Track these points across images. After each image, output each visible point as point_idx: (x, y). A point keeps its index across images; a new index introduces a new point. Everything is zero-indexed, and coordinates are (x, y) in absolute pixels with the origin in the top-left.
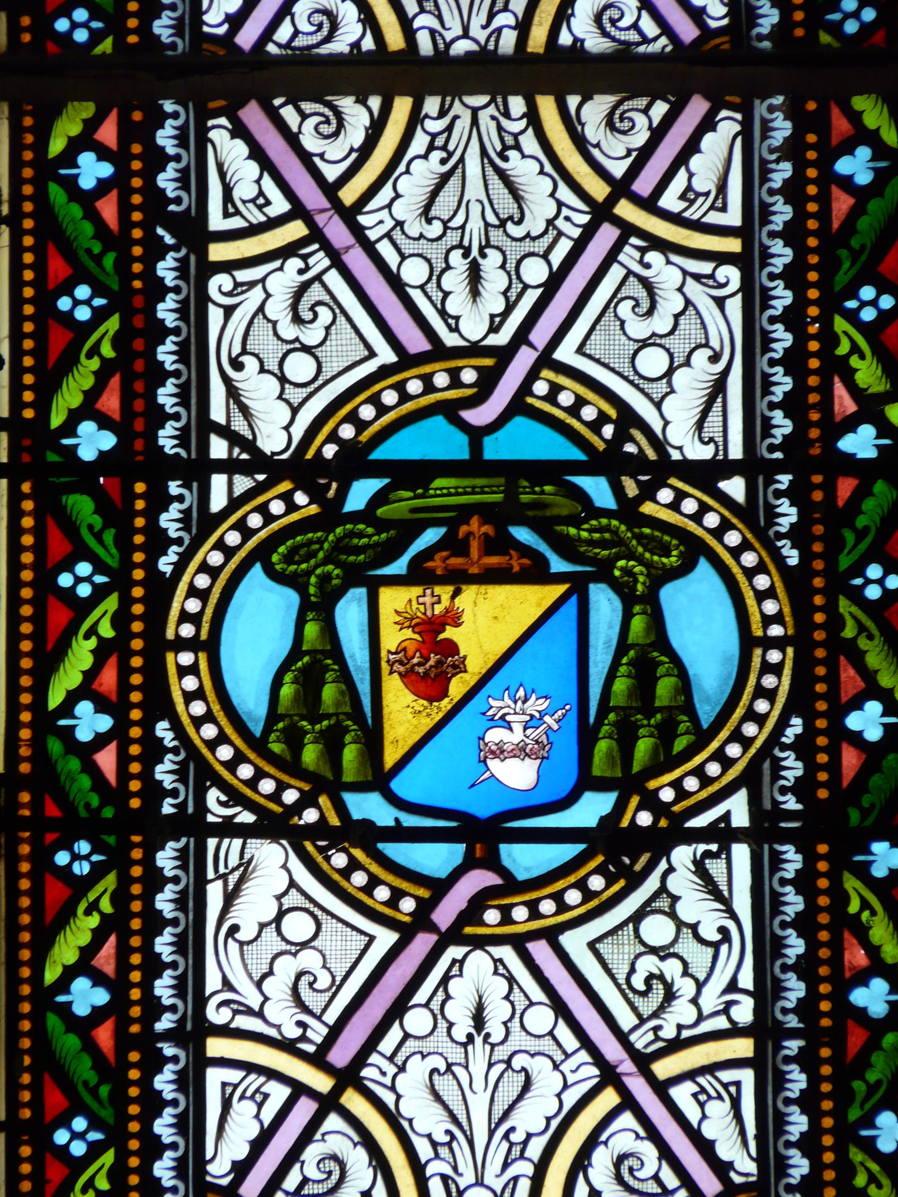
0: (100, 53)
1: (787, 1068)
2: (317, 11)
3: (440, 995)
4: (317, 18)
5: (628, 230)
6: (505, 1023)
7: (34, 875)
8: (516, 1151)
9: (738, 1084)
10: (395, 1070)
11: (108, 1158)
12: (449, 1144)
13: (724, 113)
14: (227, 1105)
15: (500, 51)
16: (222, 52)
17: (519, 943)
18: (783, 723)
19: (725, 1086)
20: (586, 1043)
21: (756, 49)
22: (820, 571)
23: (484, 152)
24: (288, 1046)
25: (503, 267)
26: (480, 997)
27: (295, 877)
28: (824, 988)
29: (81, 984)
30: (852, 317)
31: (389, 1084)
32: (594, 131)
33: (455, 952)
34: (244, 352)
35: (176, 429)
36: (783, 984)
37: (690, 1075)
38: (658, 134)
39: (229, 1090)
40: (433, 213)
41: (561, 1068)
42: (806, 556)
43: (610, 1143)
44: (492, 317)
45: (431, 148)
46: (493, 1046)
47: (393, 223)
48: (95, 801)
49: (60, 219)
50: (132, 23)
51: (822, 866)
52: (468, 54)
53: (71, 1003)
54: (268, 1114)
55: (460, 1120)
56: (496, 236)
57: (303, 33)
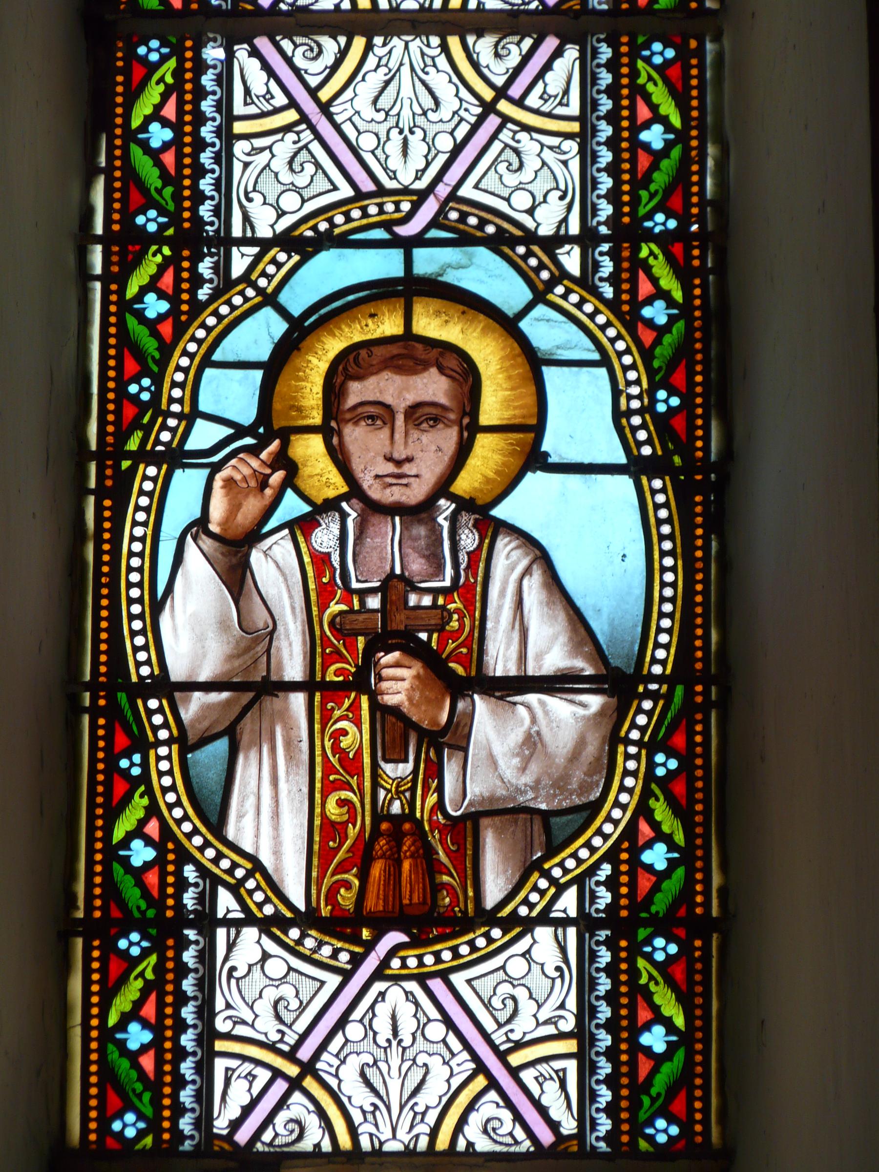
1: (598, 70)
3: (430, 158)
4: (291, 1126)
5: (506, 119)
7: (117, 402)
8: (419, 1117)
9: (564, 1070)
10: (339, 1062)
11: (153, 959)
12: (373, 1113)
13: (225, 1132)
14: (227, 1082)
17: (422, 979)
18: (596, 867)
19: (556, 1072)
20: (337, 127)
23: (388, 1108)
24: (271, 1047)
25: (424, 140)
26: (405, 162)
27: (288, 215)
28: (624, 1012)
30: (649, 957)
31: (463, 102)
32: (312, 1122)
33: (379, 986)
36: (596, 1037)
37: (277, 111)
38: (526, 59)
40: (422, 1071)
42: (617, 292)
43: (480, 1110)
44: (417, 171)
45: (424, 1114)
46: (404, 1049)
47: (354, 112)
48: (143, 906)
51: (626, 188)
56: (420, 121)
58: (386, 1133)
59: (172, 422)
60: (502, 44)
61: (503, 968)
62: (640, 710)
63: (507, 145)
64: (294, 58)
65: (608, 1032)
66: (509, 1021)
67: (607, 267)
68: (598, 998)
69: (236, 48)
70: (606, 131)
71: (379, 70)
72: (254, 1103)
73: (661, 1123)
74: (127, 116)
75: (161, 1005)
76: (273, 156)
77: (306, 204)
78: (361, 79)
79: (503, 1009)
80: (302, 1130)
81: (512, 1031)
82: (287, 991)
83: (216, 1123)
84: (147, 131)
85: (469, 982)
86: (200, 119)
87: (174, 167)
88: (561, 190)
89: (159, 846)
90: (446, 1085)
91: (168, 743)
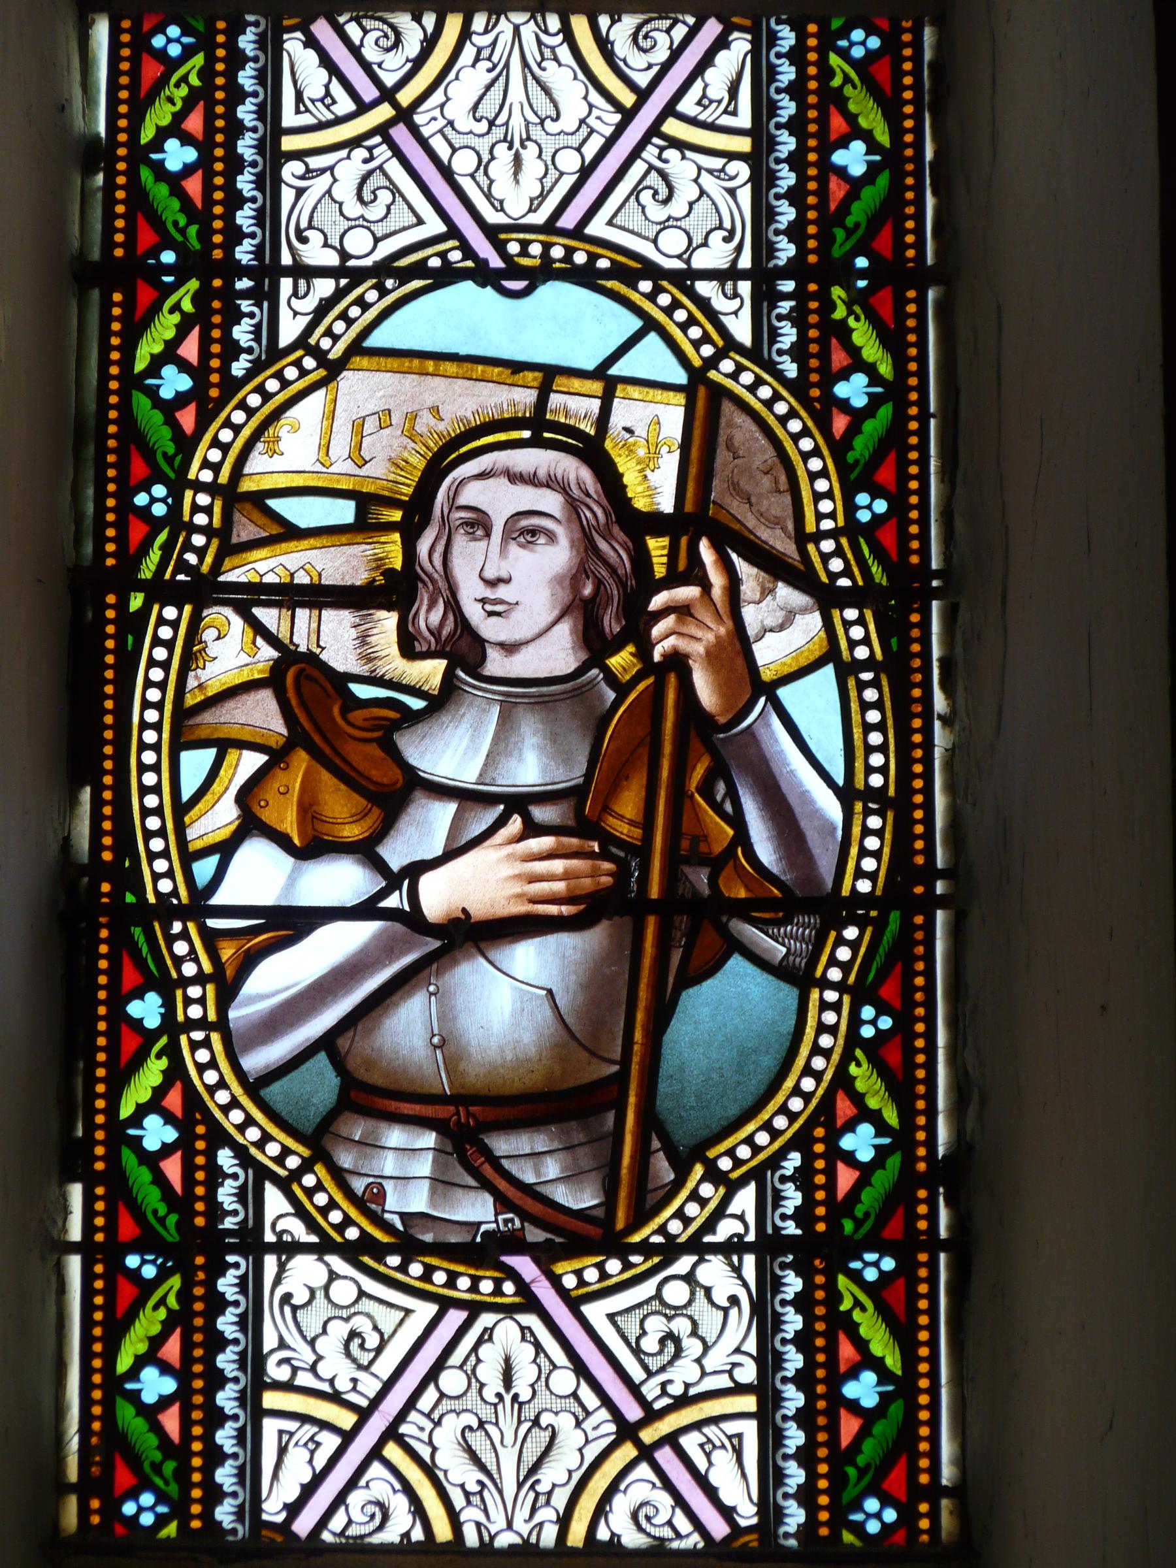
0: (165, 1536)
2: (370, 1502)
3: (548, 182)
4: (371, 1509)
6: (532, 1386)
8: (485, 53)
9: (740, 1436)
10: (587, 121)
13: (736, 35)
14: (282, 1451)
15: (542, 1544)
16: (279, 1539)
19: (730, 1438)
20: (606, 1401)
21: (783, 1547)
22: (812, 358)
23: (525, 64)
29: (150, 1374)
30: (844, 54)
31: (427, 1440)
34: (310, 227)
35: (252, 246)
39: (731, 108)
40: (548, 1434)
41: (583, 1426)
42: (803, 370)
46: (521, 1404)
47: (445, 122)
49: (130, 1183)
50: (221, 38)
52: (511, 1546)
53: (140, 1391)
54: (320, 1462)
55: (489, 1468)
56: (486, 1413)
57: (357, 1523)
58: (529, 32)
59: (198, 540)
60: (644, 30)
61: (377, 240)
62: (840, 941)
63: (651, 167)
64: (363, 49)
65: (799, 1388)
66: (370, 173)
67: (226, 1195)
68: (253, 200)
69: (285, 37)
70: (787, 143)
71: (479, 65)
72: (318, 1479)
73: (872, 1505)
74: (114, 1098)
75: (187, 1346)
76: (335, 180)
77: (380, 244)
78: (454, 77)
79: (379, 188)
80: (385, 1517)
81: (366, 161)
82: (657, 213)
83: (748, 47)
84: (140, 1126)
85: (420, 222)
86: (236, 129)
87: (200, 198)
88: (725, 230)
89: (183, 1124)
90: (450, 94)
91: (820, 536)
